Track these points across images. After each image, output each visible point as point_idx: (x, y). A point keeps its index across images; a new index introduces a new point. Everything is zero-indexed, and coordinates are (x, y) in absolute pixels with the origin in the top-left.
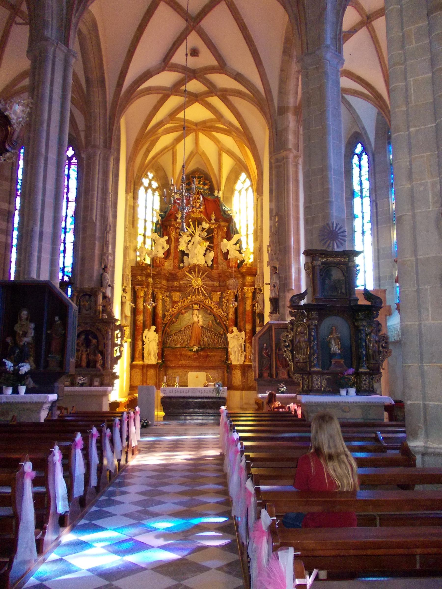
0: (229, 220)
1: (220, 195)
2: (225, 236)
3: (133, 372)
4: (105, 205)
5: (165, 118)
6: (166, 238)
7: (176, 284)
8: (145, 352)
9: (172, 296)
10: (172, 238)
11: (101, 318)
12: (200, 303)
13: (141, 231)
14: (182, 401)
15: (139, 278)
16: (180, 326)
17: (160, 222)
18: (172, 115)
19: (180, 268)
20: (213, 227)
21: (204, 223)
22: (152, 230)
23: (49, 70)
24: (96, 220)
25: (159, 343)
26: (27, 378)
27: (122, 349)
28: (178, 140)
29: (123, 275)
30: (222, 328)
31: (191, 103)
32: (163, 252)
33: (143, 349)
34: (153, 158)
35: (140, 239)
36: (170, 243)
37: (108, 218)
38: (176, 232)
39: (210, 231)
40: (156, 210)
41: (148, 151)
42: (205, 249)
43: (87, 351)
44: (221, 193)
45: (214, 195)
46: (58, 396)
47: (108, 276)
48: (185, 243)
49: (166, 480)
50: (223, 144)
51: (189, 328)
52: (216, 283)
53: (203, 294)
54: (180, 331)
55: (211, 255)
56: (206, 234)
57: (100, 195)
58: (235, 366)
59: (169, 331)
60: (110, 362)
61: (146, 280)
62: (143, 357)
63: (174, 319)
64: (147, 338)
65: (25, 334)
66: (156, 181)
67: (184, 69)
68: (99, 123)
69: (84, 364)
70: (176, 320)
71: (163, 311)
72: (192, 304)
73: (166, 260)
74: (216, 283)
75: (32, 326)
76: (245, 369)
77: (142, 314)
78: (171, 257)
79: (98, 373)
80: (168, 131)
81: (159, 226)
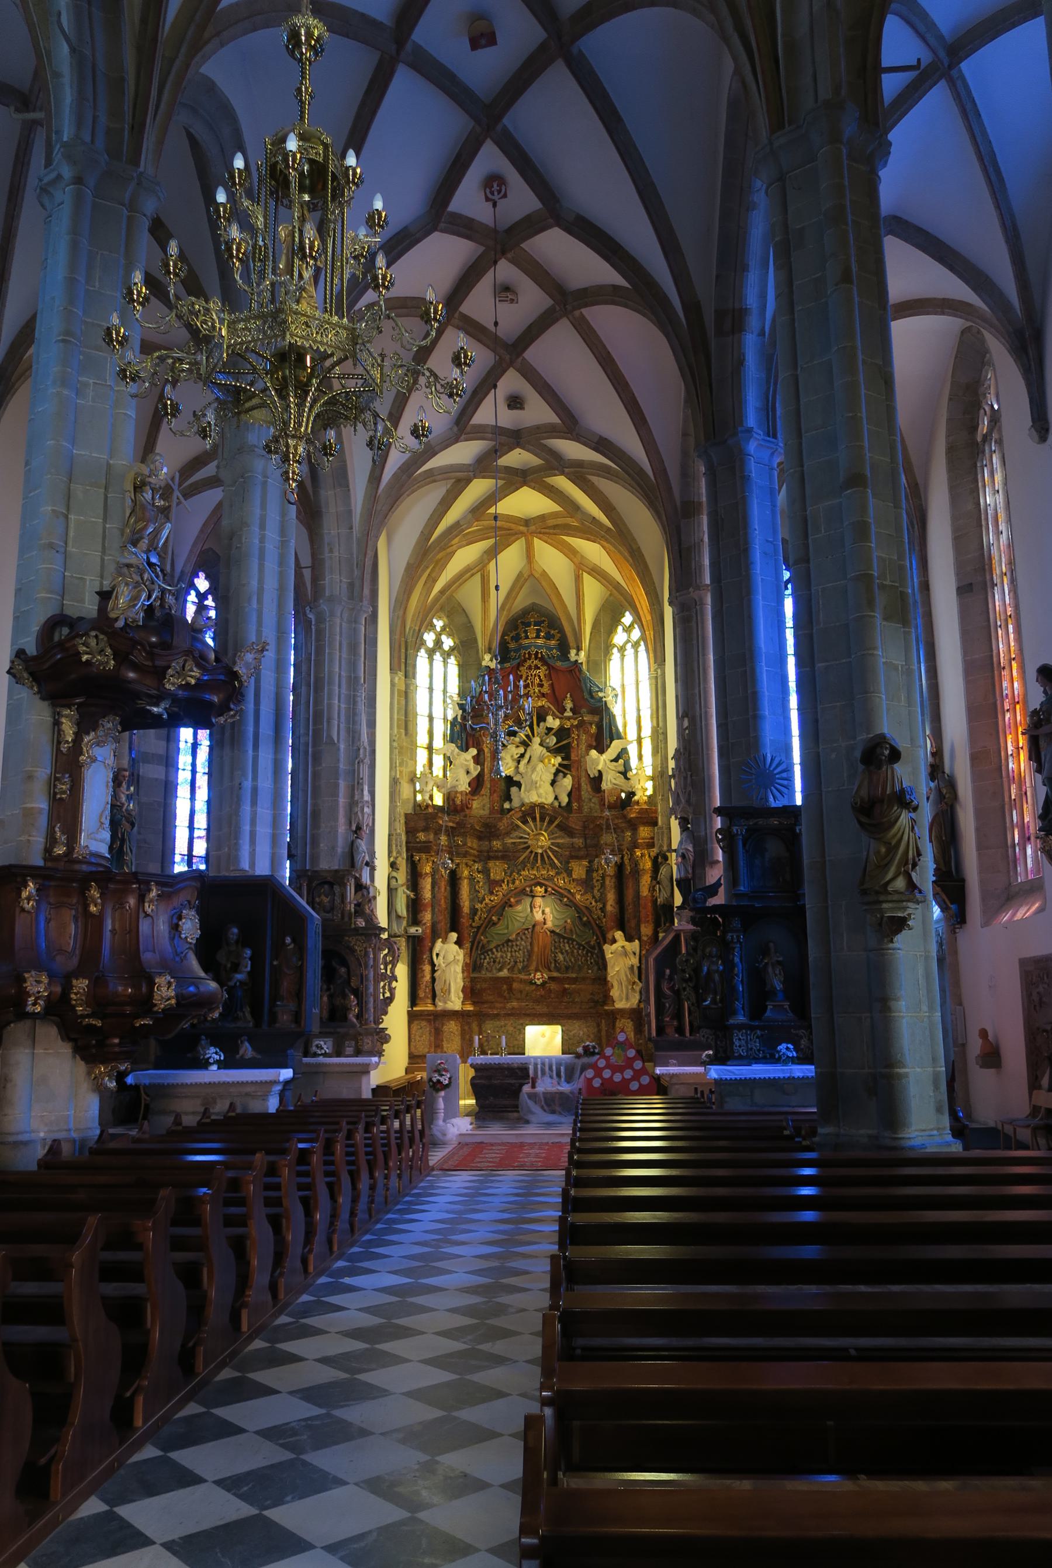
0: (600, 711)
1: (582, 657)
2: (594, 744)
3: (415, 1026)
4: (353, 709)
5: (464, 517)
6: (473, 751)
7: (497, 844)
8: (437, 988)
9: (489, 870)
10: (486, 750)
11: (353, 926)
12: (547, 883)
13: (422, 739)
14: (511, 1084)
15: (422, 836)
16: (506, 931)
17: (459, 720)
18: (478, 510)
19: (503, 812)
20: (567, 725)
21: (550, 718)
22: (445, 736)
23: (258, 502)
25: (466, 968)
27: (394, 984)
28: (493, 553)
29: (389, 835)
30: (593, 933)
31: (514, 487)
32: (468, 781)
33: (433, 980)
34: (442, 592)
35: (422, 756)
36: (482, 760)
37: (360, 734)
39: (562, 733)
40: (451, 697)
42: (553, 770)
44: (582, 654)
45: (568, 659)
47: (362, 845)
48: (513, 760)
49: (478, 1207)
50: (582, 557)
51: (524, 934)
52: (579, 841)
53: (553, 866)
54: (509, 941)
55: (567, 782)
56: (555, 740)
57: (344, 691)
58: (622, 1011)
60: (372, 1010)
61: (435, 840)
62: (434, 996)
63: (494, 918)
64: (441, 958)
65: (236, 968)
66: (449, 635)
67: (498, 431)
70: (499, 919)
71: (471, 900)
72: (530, 886)
73: (476, 798)
74: (579, 841)
75: (248, 952)
76: (637, 1015)
77: (429, 909)
78: (485, 791)
79: (352, 1031)
81: (457, 728)
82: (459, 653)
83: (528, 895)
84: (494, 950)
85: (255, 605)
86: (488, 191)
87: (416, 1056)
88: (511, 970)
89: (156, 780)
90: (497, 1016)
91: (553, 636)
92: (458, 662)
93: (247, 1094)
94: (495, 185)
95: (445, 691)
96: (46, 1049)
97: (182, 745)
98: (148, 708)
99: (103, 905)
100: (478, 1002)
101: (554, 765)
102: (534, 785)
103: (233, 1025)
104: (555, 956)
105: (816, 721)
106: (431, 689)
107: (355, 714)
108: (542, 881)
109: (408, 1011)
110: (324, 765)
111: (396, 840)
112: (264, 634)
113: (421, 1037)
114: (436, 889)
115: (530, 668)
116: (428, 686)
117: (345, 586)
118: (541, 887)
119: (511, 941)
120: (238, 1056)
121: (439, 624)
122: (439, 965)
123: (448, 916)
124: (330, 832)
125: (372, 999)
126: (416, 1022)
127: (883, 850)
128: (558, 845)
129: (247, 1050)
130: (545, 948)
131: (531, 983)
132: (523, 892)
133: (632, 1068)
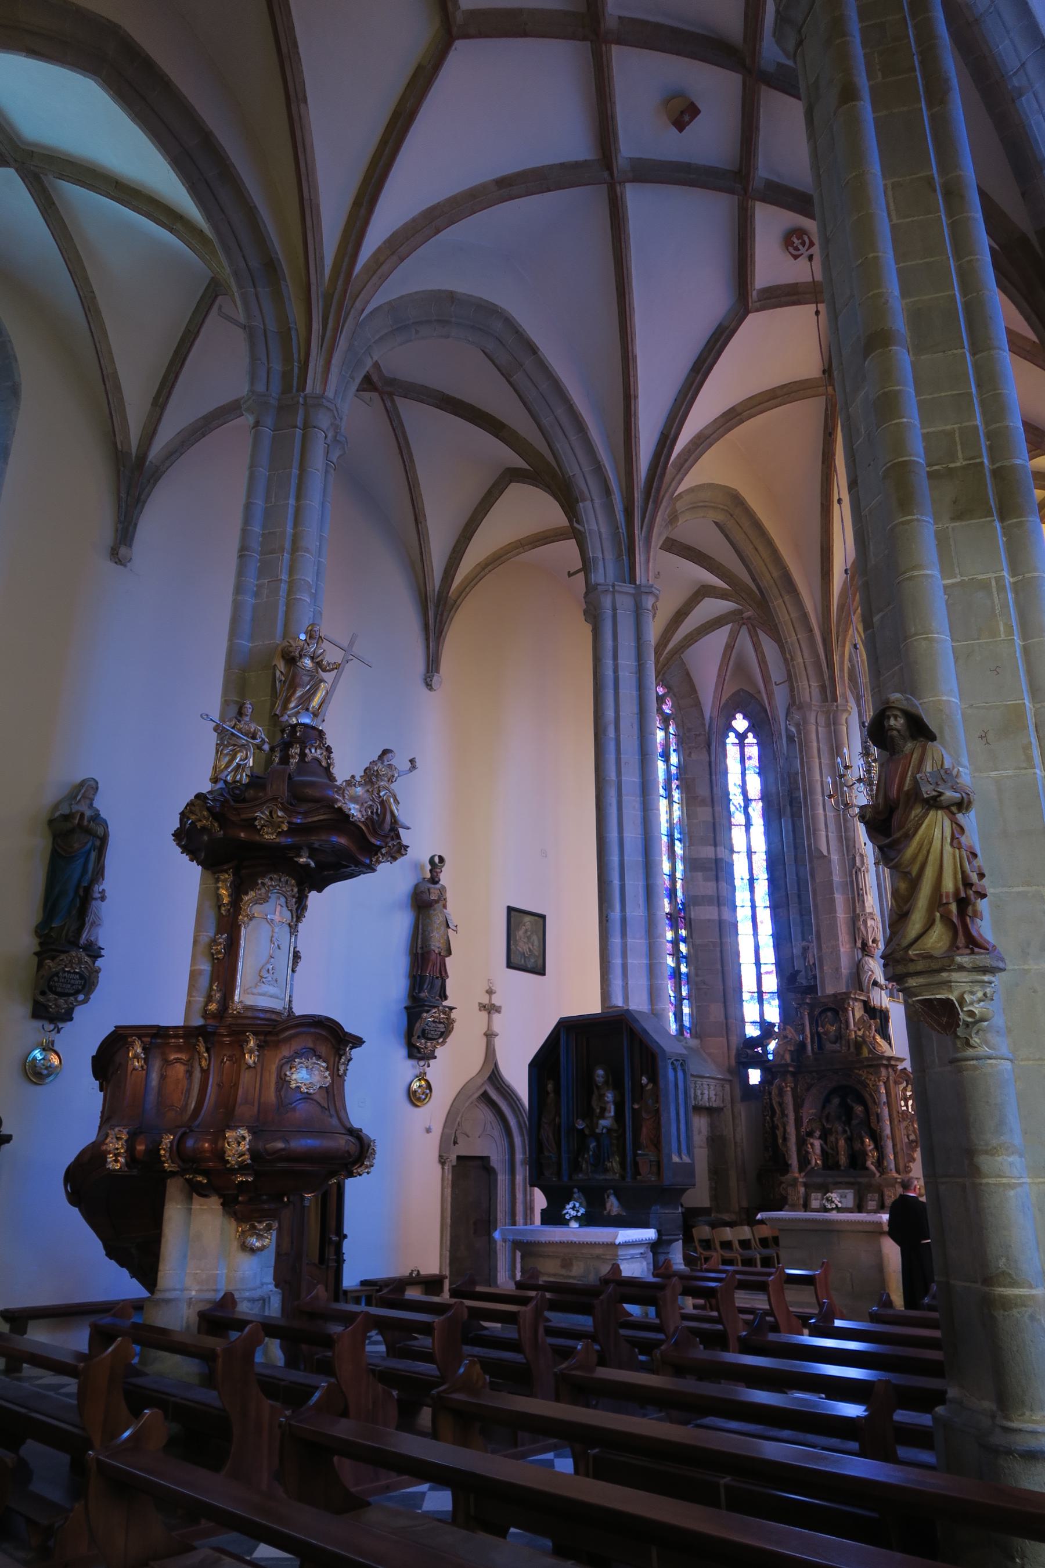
26: (608, 1197)
43: (845, 1132)
46: (659, 1232)
60: (892, 1157)
65: (602, 1116)
68: (802, 658)
69: (843, 1159)
86: (791, 249)
89: (709, 920)
93: (598, 1257)
94: (795, 240)
96: (201, 1205)
97: (738, 883)
99: (146, 1060)
103: (602, 1177)
117: (817, 690)
120: (605, 1212)
124: (831, 953)
125: (890, 1144)
129: (613, 1205)
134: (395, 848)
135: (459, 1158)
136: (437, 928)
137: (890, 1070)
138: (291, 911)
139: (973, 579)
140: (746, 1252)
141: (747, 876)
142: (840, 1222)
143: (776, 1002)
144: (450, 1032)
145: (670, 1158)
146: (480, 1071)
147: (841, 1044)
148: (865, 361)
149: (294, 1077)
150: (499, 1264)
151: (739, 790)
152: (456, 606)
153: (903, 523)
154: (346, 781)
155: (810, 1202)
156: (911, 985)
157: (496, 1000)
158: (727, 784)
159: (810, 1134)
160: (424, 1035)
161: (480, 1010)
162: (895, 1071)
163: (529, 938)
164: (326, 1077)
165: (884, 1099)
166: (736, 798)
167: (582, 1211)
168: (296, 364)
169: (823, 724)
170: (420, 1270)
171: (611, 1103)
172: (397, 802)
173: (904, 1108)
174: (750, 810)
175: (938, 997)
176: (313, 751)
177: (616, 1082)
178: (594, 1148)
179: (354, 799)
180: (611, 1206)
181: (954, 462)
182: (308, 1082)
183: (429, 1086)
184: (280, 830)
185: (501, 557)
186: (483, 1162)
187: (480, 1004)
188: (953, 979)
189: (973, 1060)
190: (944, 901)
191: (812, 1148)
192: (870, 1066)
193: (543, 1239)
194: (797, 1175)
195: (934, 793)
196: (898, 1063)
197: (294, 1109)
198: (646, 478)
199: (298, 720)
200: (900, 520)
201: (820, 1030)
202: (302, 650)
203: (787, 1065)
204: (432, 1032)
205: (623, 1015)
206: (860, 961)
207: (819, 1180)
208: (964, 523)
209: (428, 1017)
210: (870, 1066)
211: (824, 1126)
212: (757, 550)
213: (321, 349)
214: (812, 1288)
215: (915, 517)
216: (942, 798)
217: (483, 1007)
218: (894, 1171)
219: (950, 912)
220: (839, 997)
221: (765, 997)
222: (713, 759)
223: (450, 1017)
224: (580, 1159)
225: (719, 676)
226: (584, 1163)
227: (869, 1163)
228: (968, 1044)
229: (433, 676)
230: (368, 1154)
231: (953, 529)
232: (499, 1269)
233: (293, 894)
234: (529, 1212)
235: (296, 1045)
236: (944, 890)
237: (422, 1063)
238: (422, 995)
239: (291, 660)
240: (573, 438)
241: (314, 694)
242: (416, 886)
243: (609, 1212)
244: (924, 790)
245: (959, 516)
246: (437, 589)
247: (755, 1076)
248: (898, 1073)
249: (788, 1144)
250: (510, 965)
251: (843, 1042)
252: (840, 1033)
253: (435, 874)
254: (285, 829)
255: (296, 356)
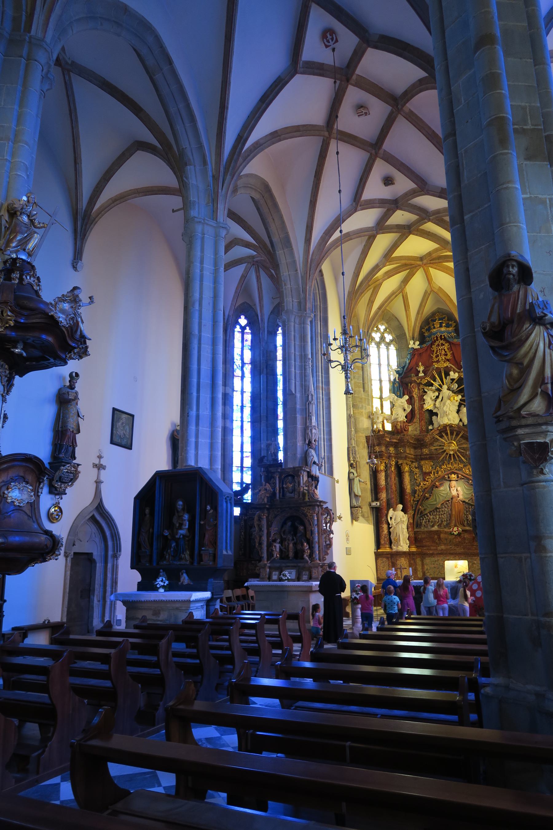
3: (379, 561)
5: (381, 261)
6: (406, 397)
7: (426, 451)
10: (415, 396)
12: (458, 472)
13: (376, 393)
15: (377, 449)
16: (435, 503)
18: (387, 256)
21: (452, 373)
23: (198, 248)
24: (295, 392)
26: (182, 574)
28: (406, 281)
31: (405, 237)
33: (390, 533)
34: (379, 308)
35: (376, 403)
38: (419, 389)
39: (460, 381)
41: (371, 302)
42: (457, 404)
43: (293, 539)
46: (212, 593)
48: (432, 400)
51: (447, 504)
53: (461, 461)
54: (437, 508)
59: (423, 509)
60: (317, 553)
62: (391, 543)
63: (426, 495)
64: (393, 520)
65: (180, 527)
66: (389, 333)
69: (291, 554)
70: (430, 495)
71: (411, 485)
72: (448, 474)
77: (384, 491)
80: (389, 275)
82: (396, 342)
83: (447, 480)
84: (429, 514)
85: (197, 307)
86: (325, 40)
87: (381, 579)
88: (439, 526)
90: (432, 555)
91: (451, 325)
92: (396, 348)
93: (177, 609)
94: (328, 36)
95: (389, 365)
97: (235, 407)
98: (12, 350)
100: (420, 546)
101: (457, 401)
102: (445, 414)
104: (467, 517)
105: (467, 270)
106: (380, 365)
107: (305, 376)
108: (455, 471)
109: (375, 552)
110: (288, 407)
111: (352, 451)
112: (202, 324)
113: (383, 568)
114: (389, 479)
115: (438, 345)
116: (378, 363)
117: (296, 304)
118: (455, 475)
119: (439, 509)
120: (180, 583)
121: (382, 328)
122: (392, 524)
123: (398, 495)
125: (317, 546)
126: (380, 559)
127: (515, 372)
128: (463, 449)
129: (185, 579)
130: (459, 512)
131: (451, 534)
132: (443, 478)
133: (476, 591)
134: (82, 350)
135: (75, 553)
136: (72, 416)
137: (320, 508)
138: (4, 385)
139: (536, 197)
140: (230, 603)
141: (240, 405)
142: (288, 586)
143: (250, 473)
144: (76, 479)
145: (222, 552)
146: (91, 503)
147: (294, 493)
148: (475, 53)
149: (10, 495)
150: (94, 614)
151: (240, 357)
152: (95, 222)
153: (502, 154)
154: (58, 298)
155: (272, 577)
156: (520, 433)
157: (103, 462)
158: (233, 354)
159: (275, 541)
160: (60, 480)
161: (93, 467)
162: (322, 508)
163: (124, 427)
164: (32, 496)
165: (316, 523)
166: (237, 362)
167: (167, 582)
168: (24, 13)
169: (298, 323)
170: (50, 619)
171: (186, 521)
172: (83, 322)
173: (325, 528)
174: (244, 369)
175: (538, 441)
176: (28, 277)
177: (190, 508)
178: (174, 546)
179: (63, 311)
180: (184, 579)
181: (526, 125)
182: (19, 499)
183: (61, 511)
184: (8, 325)
185: (125, 197)
186: (88, 557)
187: (93, 463)
188: (550, 430)
189: (543, 482)
190: (546, 382)
191: (275, 548)
192: (310, 505)
193: (143, 599)
194: (266, 562)
195: (542, 314)
196: (324, 504)
197: (9, 517)
198: (227, 160)
199: (17, 256)
200: (501, 152)
201: (284, 486)
202: (22, 209)
203: (265, 504)
204: (66, 479)
205: (197, 470)
206: (307, 451)
207: (278, 565)
208: (532, 163)
209: (64, 469)
210: (310, 505)
211: (281, 536)
212: (274, 220)
213: (43, 8)
214: (297, 621)
215: (510, 151)
216: (546, 318)
217: (95, 466)
218: (318, 560)
219: (547, 388)
220: (296, 469)
221: (244, 469)
222: (228, 338)
223: (77, 470)
224: (165, 553)
225: (236, 292)
226: (167, 555)
227: (305, 556)
228: (542, 472)
229: (78, 262)
230: (58, 547)
231: (526, 165)
232: (94, 618)
233: (6, 374)
234: (114, 584)
235: (12, 473)
236: (546, 375)
237: (57, 497)
238: (61, 456)
239: (13, 213)
240: (188, 125)
241: (29, 240)
242: (60, 390)
243: (182, 582)
244: (537, 311)
245: (529, 158)
246: (84, 208)
247: (237, 511)
248: (323, 509)
249: (263, 546)
250: (112, 442)
251: (296, 493)
252: (295, 488)
253: (73, 383)
254: (12, 325)
255: (24, 7)
